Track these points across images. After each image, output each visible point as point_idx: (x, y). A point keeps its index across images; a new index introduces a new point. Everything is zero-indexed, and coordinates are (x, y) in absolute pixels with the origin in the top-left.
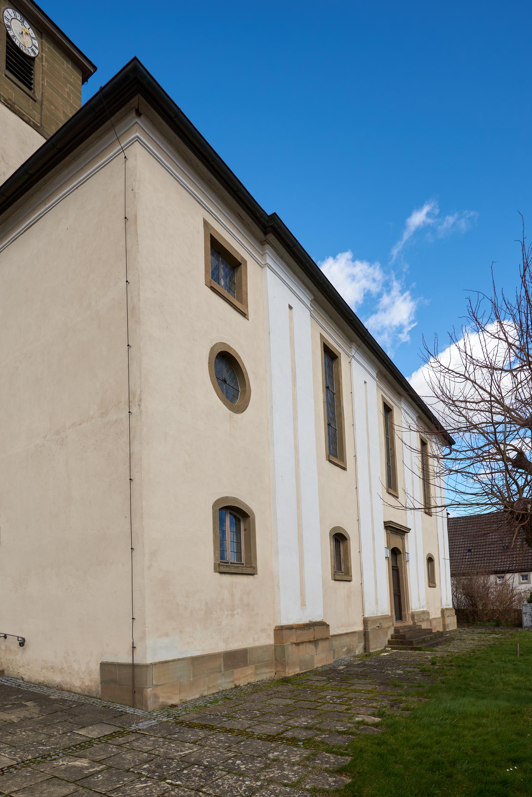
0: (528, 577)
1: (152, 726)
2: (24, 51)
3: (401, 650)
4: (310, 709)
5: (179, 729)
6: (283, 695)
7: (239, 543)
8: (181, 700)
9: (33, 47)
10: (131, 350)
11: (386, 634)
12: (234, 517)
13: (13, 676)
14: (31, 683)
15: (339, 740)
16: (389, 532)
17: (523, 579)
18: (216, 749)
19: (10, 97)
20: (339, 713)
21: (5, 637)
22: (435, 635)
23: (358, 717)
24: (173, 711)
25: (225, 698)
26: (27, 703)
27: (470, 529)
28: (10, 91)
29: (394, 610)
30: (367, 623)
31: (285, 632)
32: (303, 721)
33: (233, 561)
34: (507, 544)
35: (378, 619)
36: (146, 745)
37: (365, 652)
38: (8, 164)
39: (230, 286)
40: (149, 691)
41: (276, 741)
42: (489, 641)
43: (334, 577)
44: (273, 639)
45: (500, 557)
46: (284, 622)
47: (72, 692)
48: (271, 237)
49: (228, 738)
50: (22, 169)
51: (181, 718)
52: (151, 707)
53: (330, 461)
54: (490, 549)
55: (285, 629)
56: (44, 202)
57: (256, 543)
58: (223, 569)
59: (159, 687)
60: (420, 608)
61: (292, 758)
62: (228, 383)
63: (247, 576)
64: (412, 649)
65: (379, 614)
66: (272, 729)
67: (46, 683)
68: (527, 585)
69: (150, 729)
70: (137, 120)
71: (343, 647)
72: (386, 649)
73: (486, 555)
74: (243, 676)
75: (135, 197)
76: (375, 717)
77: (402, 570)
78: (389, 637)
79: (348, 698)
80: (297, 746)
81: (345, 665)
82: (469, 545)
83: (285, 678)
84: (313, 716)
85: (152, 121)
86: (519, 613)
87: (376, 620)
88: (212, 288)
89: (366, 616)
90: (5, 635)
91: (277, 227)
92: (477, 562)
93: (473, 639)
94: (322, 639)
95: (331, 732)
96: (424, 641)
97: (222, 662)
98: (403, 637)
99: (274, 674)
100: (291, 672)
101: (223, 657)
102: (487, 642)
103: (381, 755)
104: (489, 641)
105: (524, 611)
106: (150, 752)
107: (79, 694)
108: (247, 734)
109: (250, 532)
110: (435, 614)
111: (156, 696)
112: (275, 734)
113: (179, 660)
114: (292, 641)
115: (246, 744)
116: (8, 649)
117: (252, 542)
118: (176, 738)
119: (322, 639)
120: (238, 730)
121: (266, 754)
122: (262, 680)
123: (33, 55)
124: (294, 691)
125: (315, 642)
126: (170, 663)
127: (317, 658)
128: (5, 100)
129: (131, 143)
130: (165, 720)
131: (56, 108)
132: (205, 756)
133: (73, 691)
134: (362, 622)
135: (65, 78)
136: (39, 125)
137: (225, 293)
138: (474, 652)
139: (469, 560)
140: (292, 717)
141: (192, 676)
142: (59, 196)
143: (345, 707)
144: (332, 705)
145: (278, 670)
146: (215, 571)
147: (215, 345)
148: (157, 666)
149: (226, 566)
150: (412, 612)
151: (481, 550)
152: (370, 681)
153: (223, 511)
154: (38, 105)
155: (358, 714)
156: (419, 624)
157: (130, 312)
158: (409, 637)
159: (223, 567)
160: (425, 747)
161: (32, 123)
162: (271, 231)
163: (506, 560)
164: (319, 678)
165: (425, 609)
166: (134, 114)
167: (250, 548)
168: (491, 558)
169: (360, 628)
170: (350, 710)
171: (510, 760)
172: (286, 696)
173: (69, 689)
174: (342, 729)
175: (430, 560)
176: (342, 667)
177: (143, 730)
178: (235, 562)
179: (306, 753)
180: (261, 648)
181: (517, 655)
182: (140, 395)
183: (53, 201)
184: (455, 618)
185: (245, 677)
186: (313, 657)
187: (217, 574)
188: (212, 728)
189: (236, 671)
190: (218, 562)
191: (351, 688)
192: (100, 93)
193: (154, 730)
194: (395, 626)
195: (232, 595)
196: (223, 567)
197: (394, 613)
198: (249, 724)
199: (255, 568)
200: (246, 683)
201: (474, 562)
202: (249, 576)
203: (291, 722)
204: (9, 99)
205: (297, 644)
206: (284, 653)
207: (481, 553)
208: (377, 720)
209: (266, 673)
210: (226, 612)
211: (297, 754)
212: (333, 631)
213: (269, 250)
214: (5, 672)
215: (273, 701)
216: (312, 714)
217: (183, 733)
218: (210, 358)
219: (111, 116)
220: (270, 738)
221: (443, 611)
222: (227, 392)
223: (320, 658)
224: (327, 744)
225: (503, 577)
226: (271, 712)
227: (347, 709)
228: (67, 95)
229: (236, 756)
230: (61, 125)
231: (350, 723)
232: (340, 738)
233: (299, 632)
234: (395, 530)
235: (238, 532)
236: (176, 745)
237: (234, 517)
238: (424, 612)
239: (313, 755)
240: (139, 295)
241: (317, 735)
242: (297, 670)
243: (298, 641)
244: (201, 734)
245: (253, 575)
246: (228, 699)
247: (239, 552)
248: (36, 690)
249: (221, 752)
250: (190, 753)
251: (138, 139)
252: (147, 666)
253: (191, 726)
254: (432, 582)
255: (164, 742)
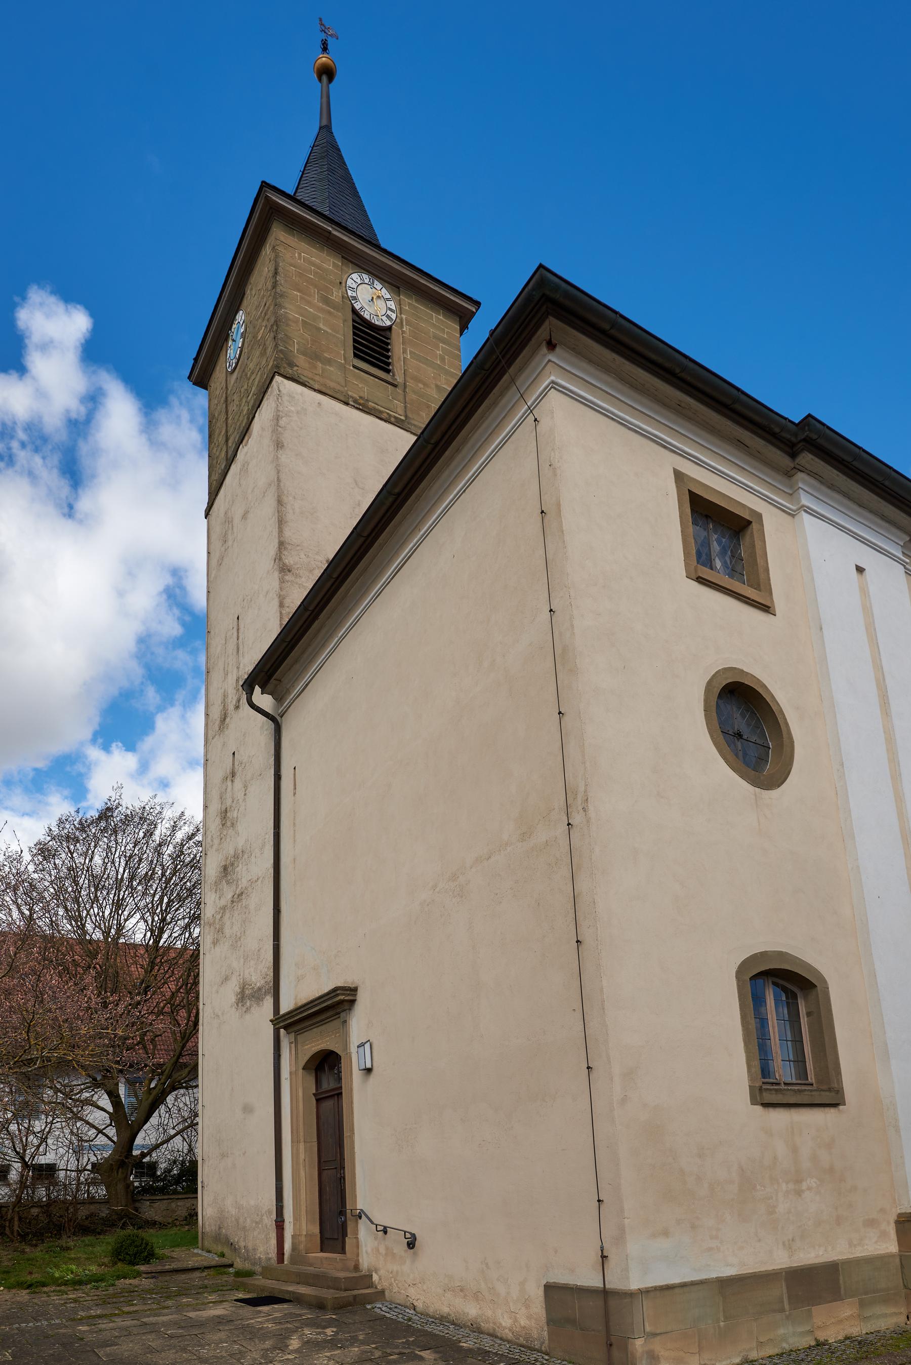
2: (377, 323)
7: (798, 1041)
9: (389, 313)
10: (565, 719)
12: (782, 990)
13: (398, 1302)
14: (427, 1315)
19: (362, 395)
21: (385, 1232)
26: (422, 1354)
28: (360, 386)
33: (789, 1080)
38: (363, 489)
39: (733, 566)
40: (639, 1345)
47: (496, 1337)
48: (806, 458)
50: (385, 491)
56: (417, 528)
58: (769, 1098)
62: (745, 737)
63: (822, 1109)
67: (453, 1317)
70: (551, 357)
74: (833, 1320)
75: (555, 475)
85: (573, 349)
88: (701, 580)
90: (385, 1228)
91: (815, 437)
97: (785, 1291)
99: (904, 1318)
107: (509, 1342)
113: (693, 1284)
116: (389, 1253)
117: (826, 1039)
122: (878, 1331)
123: (388, 323)
126: (677, 1291)
128: (355, 401)
129: (544, 395)
131: (425, 384)
133: (499, 1335)
135: (435, 337)
136: (403, 418)
137: (726, 581)
142: (439, 511)
146: (754, 1102)
147: (714, 675)
149: (776, 1090)
153: (760, 981)
154: (399, 390)
157: (560, 658)
159: (768, 1092)
161: (393, 420)
162: (806, 448)
166: (544, 349)
173: (491, 1331)
178: (794, 1081)
182: (585, 791)
183: (430, 522)
185: (838, 1322)
187: (759, 1108)
189: (815, 1310)
190: (758, 1084)
192: (491, 339)
195: (795, 1150)
196: (768, 1092)
199: (839, 1092)
200: (841, 1337)
202: (827, 1110)
204: (361, 397)
209: (885, 1316)
210: (784, 1186)
213: (804, 482)
214: (386, 1293)
218: (706, 701)
219: (509, 367)
222: (745, 755)
228: (435, 358)
230: (435, 407)
235: (794, 1020)
237: (782, 990)
240: (572, 626)
245: (835, 1105)
247: (799, 1060)
248: (437, 1330)
251: (554, 385)
252: (631, 1295)
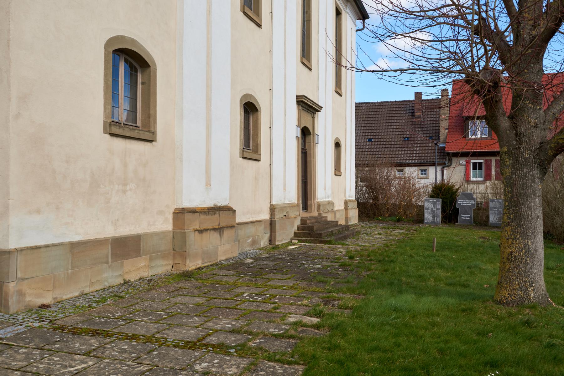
0: (427, 172)
1: (18, 334)
3: (308, 243)
4: (229, 308)
5: (61, 337)
6: (188, 293)
8: (54, 299)
11: (293, 224)
12: (130, 63)
15: (278, 346)
16: (301, 108)
17: (422, 174)
18: (121, 362)
20: (265, 313)
22: (342, 228)
23: (291, 317)
24: (46, 313)
25: (115, 296)
27: (372, 116)
29: (301, 198)
30: (274, 211)
31: (188, 216)
32: (226, 323)
34: (408, 136)
35: (285, 207)
36: (15, 360)
37: (270, 244)
41: (199, 348)
42: (397, 236)
43: (243, 154)
44: (172, 225)
45: (401, 149)
46: (186, 204)
49: (133, 347)
51: (59, 322)
52: (13, 309)
53: (245, 13)
54: (390, 140)
55: (187, 212)
57: (156, 102)
59: (26, 281)
60: (325, 198)
61: (227, 370)
64: (321, 242)
65: (287, 202)
66: (191, 334)
68: (426, 180)
69: (17, 337)
71: (249, 237)
72: (293, 241)
73: (387, 146)
74: (135, 268)
76: (311, 317)
77: (311, 153)
78: (295, 228)
79: (270, 295)
80: (229, 354)
81: (252, 258)
82: (369, 134)
83: (187, 272)
84: (236, 317)
86: (421, 208)
87: (283, 208)
89: (274, 202)
92: (377, 153)
93: (377, 236)
94: (228, 227)
95: (265, 335)
96: (332, 234)
97: (110, 251)
98: (311, 228)
100: (192, 265)
101: (111, 244)
102: (395, 237)
103: (341, 363)
104: (397, 236)
105: (426, 207)
106: (24, 369)
108: (158, 340)
109: (149, 86)
110: (339, 206)
111: (21, 294)
112: (195, 340)
113: (53, 245)
114: (195, 227)
115: (160, 353)
117: (152, 100)
118: (58, 348)
119: (228, 227)
120: (144, 336)
121: (191, 366)
122: (158, 274)
124: (200, 287)
125: (220, 230)
126: (42, 250)
127: (221, 249)
130: (36, 324)
132: (108, 371)
134: (269, 210)
138: (387, 247)
139: (370, 150)
140: (210, 319)
141: (70, 268)
143: (270, 306)
144: (254, 304)
145: (176, 262)
146: (105, 132)
148: (24, 252)
150: (318, 202)
151: (382, 140)
152: (289, 276)
155: (290, 313)
156: (324, 215)
158: (313, 230)
159: (114, 129)
160: (385, 351)
163: (406, 152)
164: (227, 272)
165: (330, 199)
167: (149, 108)
168: (392, 149)
169: (266, 216)
170: (278, 309)
171: (486, 364)
172: (192, 293)
174: (276, 332)
175: (337, 145)
176: (249, 261)
177: (7, 339)
179: (244, 363)
180: (157, 234)
181: (433, 250)
184: (357, 210)
185: (137, 269)
186: (217, 247)
187: (108, 136)
188: (107, 335)
190: (109, 121)
191: (269, 283)
193: (23, 339)
194: (301, 216)
195: (125, 166)
196: (114, 129)
197: (301, 202)
198: (157, 328)
199: (154, 133)
200: (137, 278)
201: (375, 153)
202: (146, 143)
203: (211, 324)
205: (201, 231)
206: (185, 242)
207: (382, 143)
208: (315, 320)
209: (162, 266)
211: (232, 365)
212: (239, 219)
215: (179, 299)
216: (233, 314)
217: (67, 341)
220: (190, 345)
221: (346, 203)
223: (224, 249)
224: (266, 351)
225: (402, 171)
226: (180, 313)
227: (275, 308)
229: (151, 369)
231: (284, 324)
232: (278, 342)
233: (203, 217)
234: (307, 107)
236: (61, 358)
237: (130, 63)
238: (329, 203)
239: (253, 364)
241: (249, 340)
242: (199, 263)
243: (202, 228)
244: (94, 342)
246: (119, 297)
249: (128, 366)
250: (85, 369)
253: (76, 332)
254: (338, 171)
255: (41, 355)
